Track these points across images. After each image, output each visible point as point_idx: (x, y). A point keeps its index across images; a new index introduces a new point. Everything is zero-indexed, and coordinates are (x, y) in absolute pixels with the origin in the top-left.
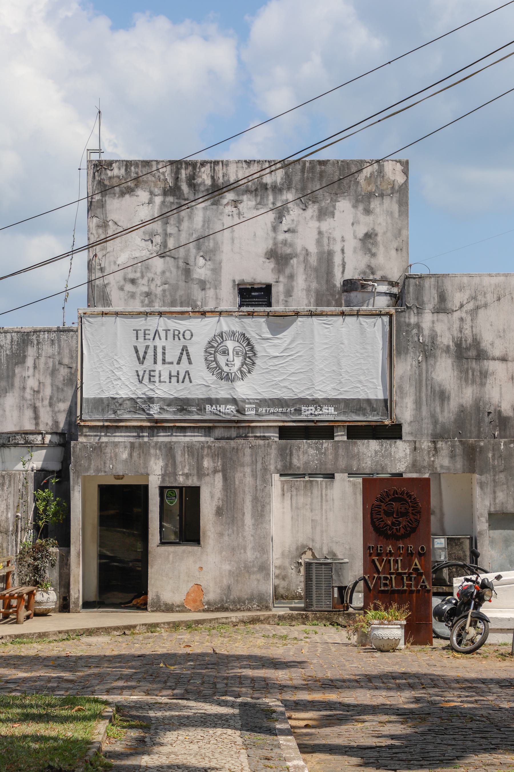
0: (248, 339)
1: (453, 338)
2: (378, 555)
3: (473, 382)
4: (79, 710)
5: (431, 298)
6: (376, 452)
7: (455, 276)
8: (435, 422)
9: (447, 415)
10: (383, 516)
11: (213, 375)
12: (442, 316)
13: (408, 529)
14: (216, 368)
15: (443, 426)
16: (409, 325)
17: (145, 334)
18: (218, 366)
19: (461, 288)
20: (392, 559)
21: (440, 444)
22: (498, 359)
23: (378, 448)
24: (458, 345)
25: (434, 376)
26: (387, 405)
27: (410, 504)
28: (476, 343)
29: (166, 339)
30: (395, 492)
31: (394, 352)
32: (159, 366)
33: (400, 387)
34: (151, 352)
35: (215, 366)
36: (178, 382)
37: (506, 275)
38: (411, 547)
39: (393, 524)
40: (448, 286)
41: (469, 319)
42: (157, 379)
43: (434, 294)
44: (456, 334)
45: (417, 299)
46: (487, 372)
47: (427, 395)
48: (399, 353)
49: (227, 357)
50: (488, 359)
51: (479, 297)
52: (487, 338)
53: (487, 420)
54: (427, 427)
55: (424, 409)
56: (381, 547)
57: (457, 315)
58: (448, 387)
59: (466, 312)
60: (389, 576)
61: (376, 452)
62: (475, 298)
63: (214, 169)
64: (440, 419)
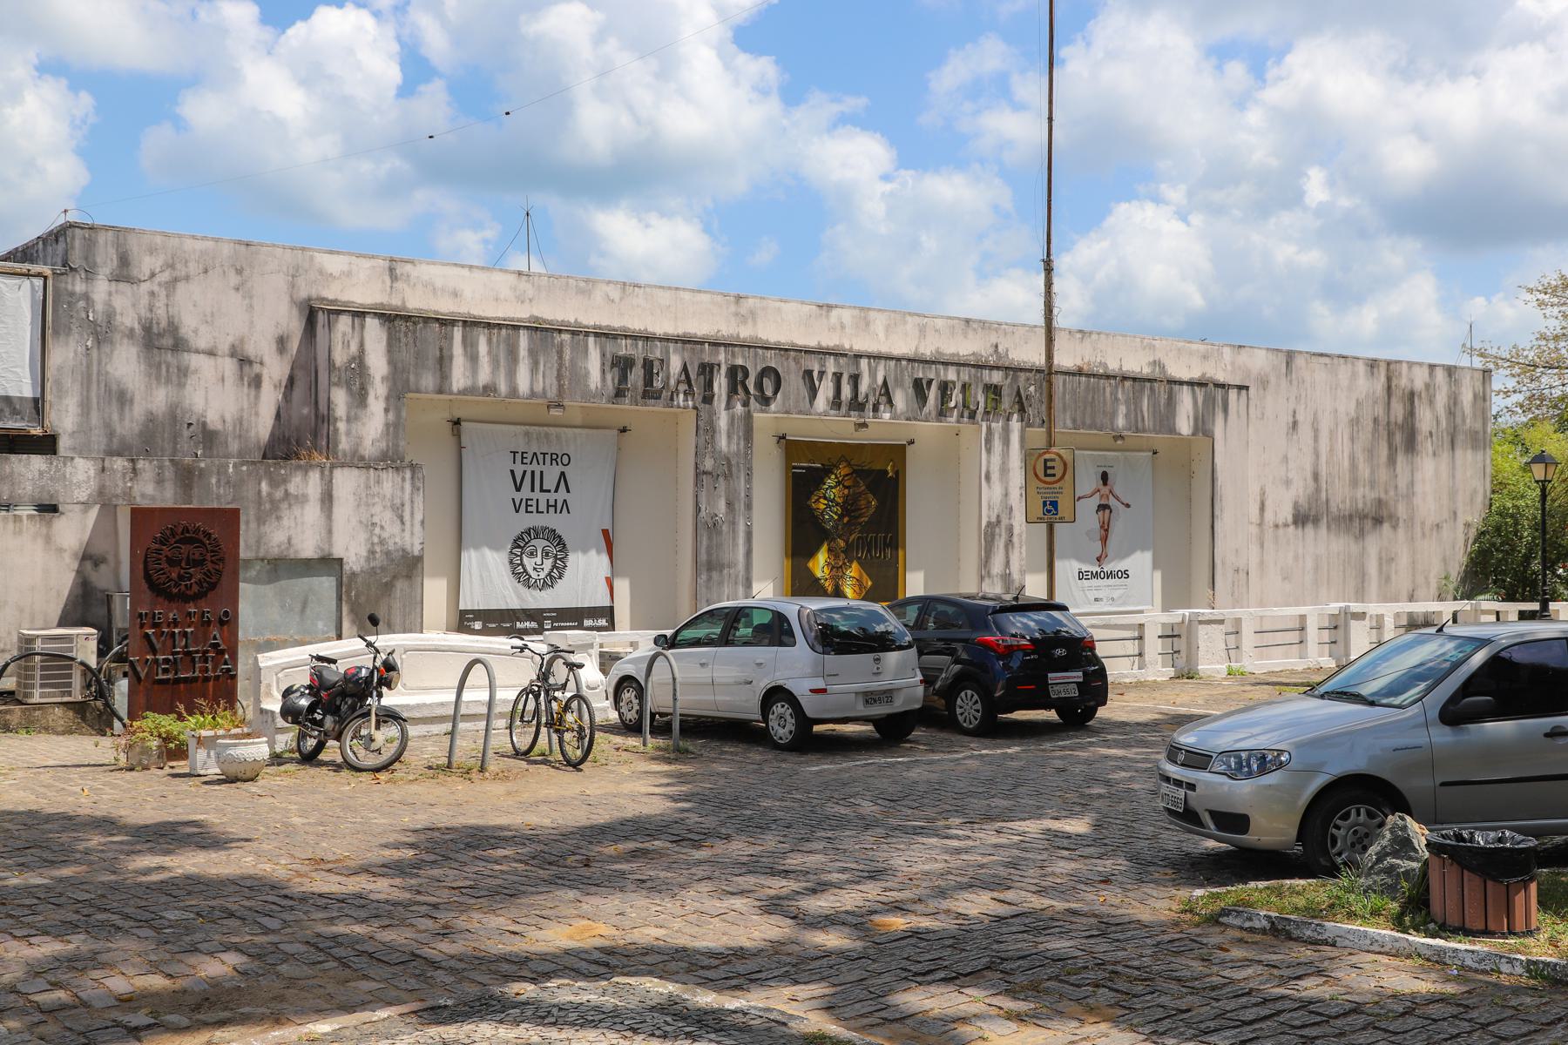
1: (140, 319)
2: (155, 625)
3: (168, 381)
5: (107, 261)
6: (41, 473)
7: (143, 232)
8: (111, 435)
9: (129, 425)
10: (165, 565)
12: (123, 286)
15: (122, 440)
16: (72, 294)
19: (152, 251)
21: (140, 464)
22: (204, 352)
23: (44, 467)
24: (147, 329)
25: (109, 368)
26: (38, 405)
28: (173, 328)
30: (186, 530)
31: (49, 332)
32: (537, 494)
33: (58, 383)
34: (528, 476)
37: (217, 240)
39: (181, 578)
40: (133, 244)
41: (163, 293)
42: (533, 509)
43: (112, 252)
44: (144, 312)
45: (86, 259)
46: (187, 368)
47: (98, 397)
48: (56, 333)
50: (189, 351)
51: (178, 266)
52: (189, 323)
53: (186, 433)
54: (98, 440)
55: (95, 419)
57: (145, 287)
58: (130, 386)
59: (160, 284)
61: (41, 473)
62: (172, 266)
64: (118, 430)
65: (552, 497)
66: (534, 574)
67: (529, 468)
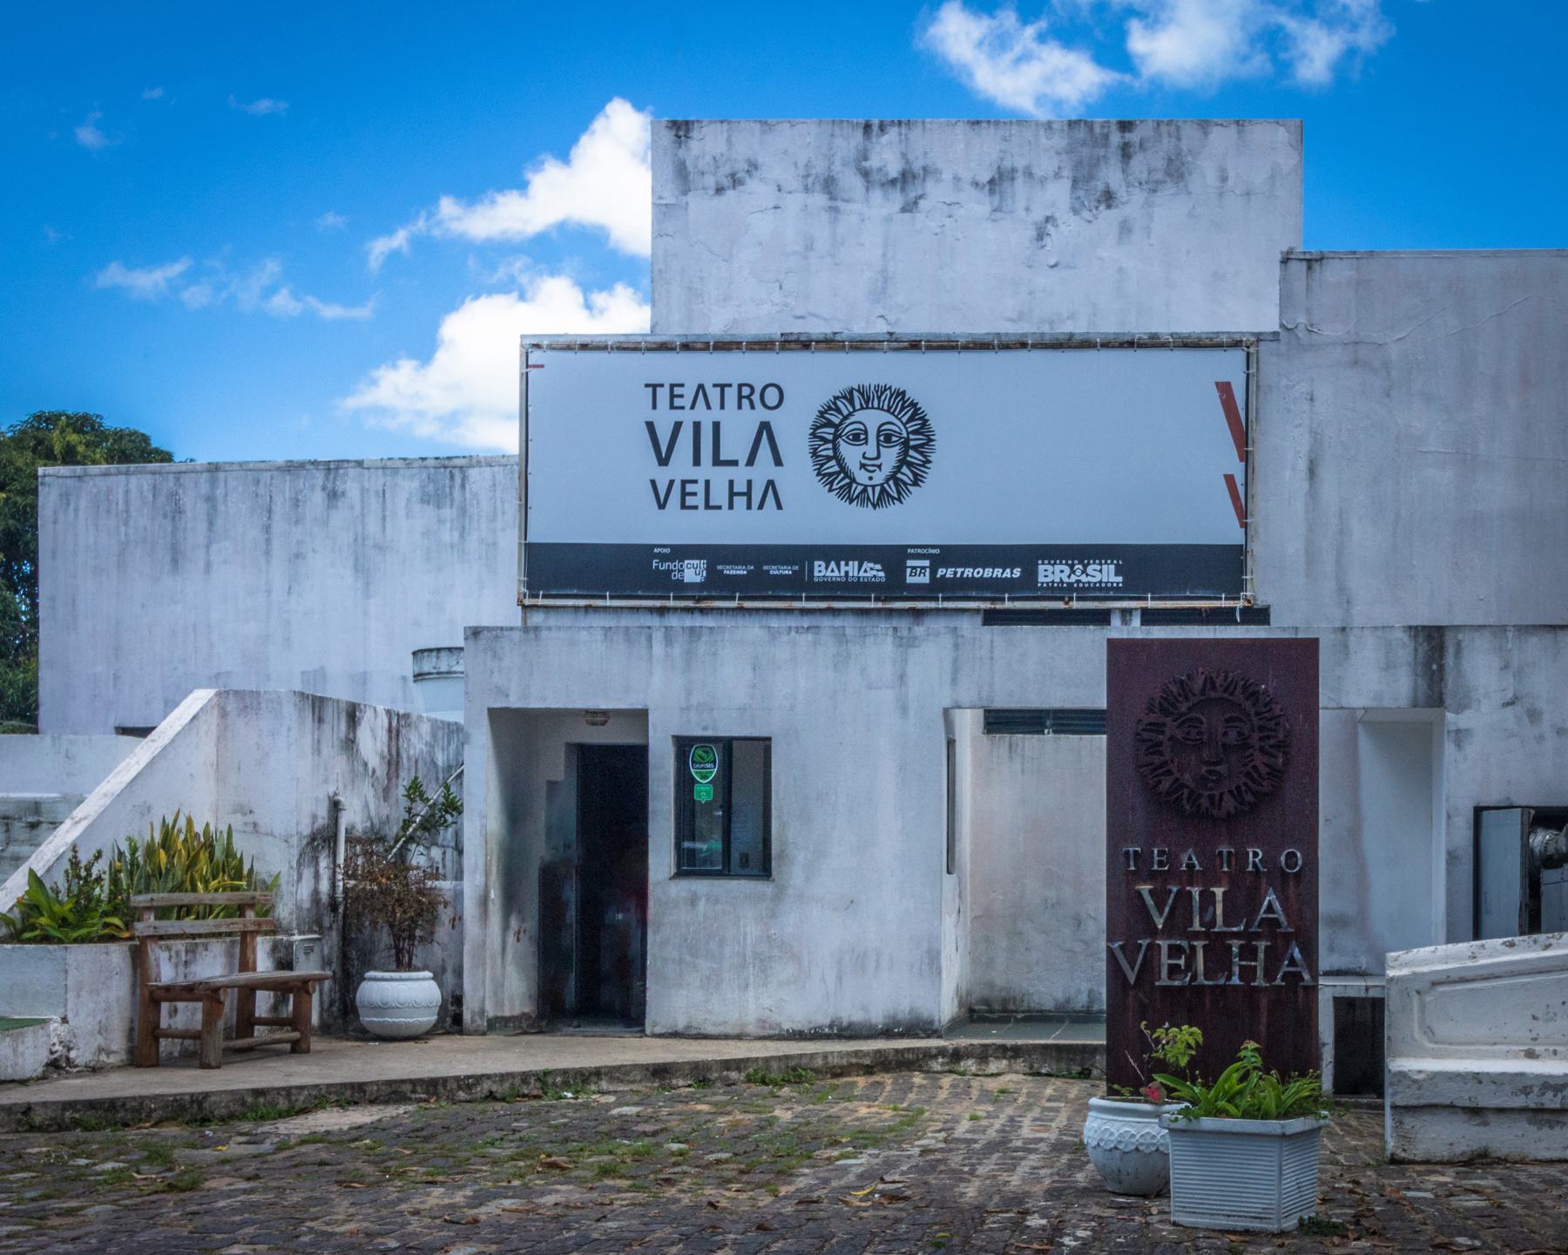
0: (914, 405)
4: (877, 1156)
11: (830, 490)
13: (1249, 798)
14: (838, 473)
17: (672, 396)
18: (843, 469)
20: (1196, 891)
27: (1254, 719)
29: (722, 407)
32: (706, 470)
34: (686, 436)
35: (836, 469)
36: (749, 507)
38: (1256, 855)
42: (699, 500)
49: (864, 448)
56: (1161, 853)
60: (1184, 944)
63: (907, 139)
65: (740, 475)
66: (862, 477)
67: (688, 417)
